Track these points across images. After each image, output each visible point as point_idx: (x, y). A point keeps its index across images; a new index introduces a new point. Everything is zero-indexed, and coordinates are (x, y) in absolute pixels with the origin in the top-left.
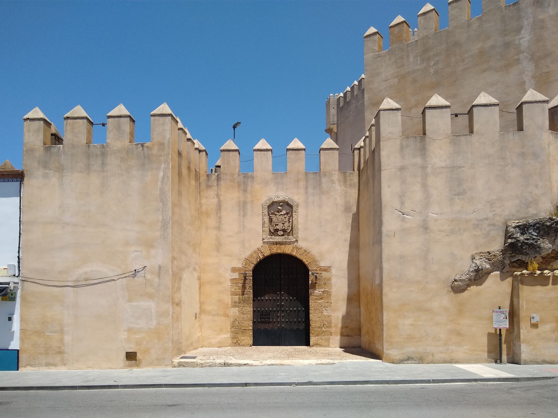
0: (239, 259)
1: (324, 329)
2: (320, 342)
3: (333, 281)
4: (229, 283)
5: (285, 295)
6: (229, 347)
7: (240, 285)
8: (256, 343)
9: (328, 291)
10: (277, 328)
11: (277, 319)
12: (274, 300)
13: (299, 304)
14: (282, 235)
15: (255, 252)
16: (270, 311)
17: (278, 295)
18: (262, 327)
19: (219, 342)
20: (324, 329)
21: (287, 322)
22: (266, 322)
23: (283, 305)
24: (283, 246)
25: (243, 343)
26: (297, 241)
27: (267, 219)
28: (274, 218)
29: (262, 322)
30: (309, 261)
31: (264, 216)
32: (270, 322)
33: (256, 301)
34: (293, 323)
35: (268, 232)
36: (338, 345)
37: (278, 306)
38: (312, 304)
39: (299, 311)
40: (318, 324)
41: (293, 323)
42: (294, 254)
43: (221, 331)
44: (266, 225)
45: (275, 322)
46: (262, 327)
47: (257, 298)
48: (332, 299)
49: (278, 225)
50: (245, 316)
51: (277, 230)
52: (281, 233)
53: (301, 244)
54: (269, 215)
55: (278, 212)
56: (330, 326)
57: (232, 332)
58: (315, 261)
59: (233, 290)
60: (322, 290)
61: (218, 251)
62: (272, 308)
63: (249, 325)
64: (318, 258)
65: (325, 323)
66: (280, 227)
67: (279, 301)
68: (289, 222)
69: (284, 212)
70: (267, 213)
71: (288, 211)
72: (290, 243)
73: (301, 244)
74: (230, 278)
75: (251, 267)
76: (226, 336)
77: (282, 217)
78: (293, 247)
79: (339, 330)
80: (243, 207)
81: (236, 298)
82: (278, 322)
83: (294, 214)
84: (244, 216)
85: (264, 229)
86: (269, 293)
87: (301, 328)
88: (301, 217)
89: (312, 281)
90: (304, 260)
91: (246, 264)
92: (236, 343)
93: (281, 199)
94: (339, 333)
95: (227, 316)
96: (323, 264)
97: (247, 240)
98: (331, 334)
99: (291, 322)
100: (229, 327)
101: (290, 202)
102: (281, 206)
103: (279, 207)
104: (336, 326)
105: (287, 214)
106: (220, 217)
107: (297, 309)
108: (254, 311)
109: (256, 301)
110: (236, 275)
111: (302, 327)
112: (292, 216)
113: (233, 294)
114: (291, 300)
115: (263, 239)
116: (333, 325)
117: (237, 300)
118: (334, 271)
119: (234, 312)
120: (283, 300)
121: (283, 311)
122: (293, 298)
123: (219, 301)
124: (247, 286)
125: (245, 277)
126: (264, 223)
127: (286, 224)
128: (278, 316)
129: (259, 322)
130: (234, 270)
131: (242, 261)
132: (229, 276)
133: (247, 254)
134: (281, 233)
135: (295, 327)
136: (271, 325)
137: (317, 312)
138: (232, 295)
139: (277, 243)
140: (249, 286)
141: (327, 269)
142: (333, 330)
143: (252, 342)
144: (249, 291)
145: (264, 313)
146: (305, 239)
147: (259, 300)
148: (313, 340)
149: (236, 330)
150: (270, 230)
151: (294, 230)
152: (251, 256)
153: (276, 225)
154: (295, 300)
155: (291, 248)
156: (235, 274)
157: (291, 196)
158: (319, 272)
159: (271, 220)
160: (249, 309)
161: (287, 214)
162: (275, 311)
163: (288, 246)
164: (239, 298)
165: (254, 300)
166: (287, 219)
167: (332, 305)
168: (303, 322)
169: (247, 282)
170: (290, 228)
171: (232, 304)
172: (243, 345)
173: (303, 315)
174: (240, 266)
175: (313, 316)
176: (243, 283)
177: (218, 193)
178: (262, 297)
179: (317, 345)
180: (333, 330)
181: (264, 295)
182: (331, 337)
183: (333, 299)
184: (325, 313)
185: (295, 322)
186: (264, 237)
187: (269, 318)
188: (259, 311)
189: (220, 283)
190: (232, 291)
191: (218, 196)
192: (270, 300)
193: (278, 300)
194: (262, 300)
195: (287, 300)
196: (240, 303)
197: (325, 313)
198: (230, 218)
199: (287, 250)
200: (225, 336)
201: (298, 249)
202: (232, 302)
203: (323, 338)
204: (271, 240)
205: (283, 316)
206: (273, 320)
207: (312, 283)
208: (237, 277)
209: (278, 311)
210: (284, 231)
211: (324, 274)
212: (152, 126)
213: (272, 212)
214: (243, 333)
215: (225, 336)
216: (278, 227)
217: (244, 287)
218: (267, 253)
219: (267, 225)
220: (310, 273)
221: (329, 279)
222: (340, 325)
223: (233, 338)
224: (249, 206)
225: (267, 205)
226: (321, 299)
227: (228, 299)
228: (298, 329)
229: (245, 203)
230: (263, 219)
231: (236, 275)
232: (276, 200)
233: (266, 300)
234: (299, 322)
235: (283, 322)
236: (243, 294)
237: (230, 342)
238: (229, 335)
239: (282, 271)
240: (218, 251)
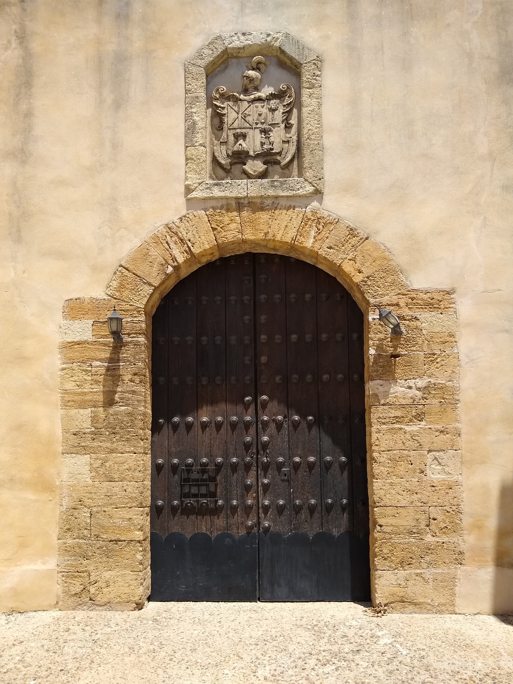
0: (95, 269)
1: (429, 538)
2: (415, 590)
3: (465, 344)
4: (57, 361)
5: (274, 406)
6: (56, 613)
7: (100, 367)
8: (165, 587)
9: (442, 388)
10: (243, 532)
11: (242, 498)
12: (234, 426)
13: (327, 442)
14: (263, 175)
15: (156, 239)
16: (219, 467)
17: (247, 406)
18: (188, 527)
19: (15, 592)
20: (429, 538)
21: (281, 510)
22: (202, 511)
23: (265, 446)
24: (264, 216)
25: (108, 593)
26: (318, 193)
27: (202, 117)
28: (231, 116)
29: (187, 511)
30: (367, 272)
31: (190, 102)
32: (216, 511)
33: (166, 430)
34: (304, 515)
35: (208, 165)
36: (486, 603)
37: (247, 446)
38: (382, 438)
39: (328, 466)
40: (406, 520)
41: (304, 515)
42: (309, 243)
43: (23, 545)
44: (199, 138)
45: (234, 509)
46: (188, 527)
47: (168, 420)
48: (463, 417)
49: (244, 136)
50: (116, 488)
51: (240, 157)
52: (255, 166)
53: (333, 205)
54: (210, 104)
55: (246, 91)
56: (453, 528)
57: (66, 550)
58: (390, 270)
59: (70, 386)
60: (421, 383)
61: (18, 239)
62: (226, 456)
63: (136, 523)
64: (401, 259)
65: (434, 512)
66: (253, 143)
67: (252, 430)
68: (288, 127)
69: (266, 91)
70: (202, 94)
71: (282, 86)
72: (292, 203)
73: (333, 205)
74: (58, 339)
75: (142, 298)
76: (43, 566)
77: (263, 109)
78: (305, 220)
79: (489, 544)
80: (113, 75)
81: (83, 418)
82: (248, 510)
83: (305, 92)
84: (118, 105)
85: (191, 151)
86: (213, 402)
87: (335, 532)
88: (332, 106)
89: (379, 348)
90: (348, 267)
91: (121, 287)
92: (83, 595)
93: (257, 38)
94: (490, 557)
95: (44, 485)
96: (420, 281)
97: (128, 198)
98: (459, 557)
99: (298, 509)
100: (54, 531)
101: (291, 50)
102: (256, 68)
103: (252, 73)
104: (478, 527)
105: (279, 95)
106: (29, 114)
107: (321, 458)
108: (157, 469)
109: (166, 430)
110: (83, 330)
111: (339, 527)
112: (297, 104)
113: (72, 401)
114: (296, 425)
115: (188, 190)
116: (466, 521)
117: (87, 425)
118: (465, 307)
119: (76, 469)
120: (265, 424)
121: (266, 468)
122: (304, 416)
123: (19, 427)
124: (126, 373)
125: (116, 334)
126: (191, 130)
127: (277, 135)
128: (248, 488)
129: (174, 510)
130: (75, 309)
131: (107, 275)
132: (55, 330)
133: (126, 248)
134: (255, 166)
135: (311, 529)
136: (220, 522)
137: (402, 468)
138: (66, 404)
139: (239, 204)
140: (132, 369)
141: (438, 301)
142: (468, 541)
143: (143, 589)
144: (137, 397)
145: (195, 476)
146: (350, 188)
147: (175, 427)
148: (385, 582)
149: (84, 542)
150: (215, 160)
151: (306, 152)
152: (143, 253)
153: (237, 137)
154: (310, 426)
155: (296, 222)
156: (77, 325)
157: (294, 30)
158: (406, 312)
159: (218, 120)
160: (134, 464)
161: (279, 95)
162: (234, 467)
163: (283, 217)
164: (94, 419)
165: (156, 428)
166: (279, 116)
167: (462, 442)
168: (344, 508)
169: (126, 353)
170: (292, 149)
171: (65, 440)
172: (108, 605)
173: (341, 480)
174: (99, 292)
175: (384, 487)
176: (111, 360)
177: (23, 28)
178: (184, 414)
179: (404, 602)
180: (468, 541)
181: (195, 408)
182: (461, 571)
183: (464, 419)
184: (435, 474)
185: (312, 509)
186: (193, 180)
187: (213, 495)
188: (174, 468)
189: (21, 359)
190: (66, 392)
191: (22, 37)
192: (219, 426)
193: (247, 426)
194: (189, 427)
195: (279, 426)
196: (96, 435)
197: (435, 474)
198: (66, 111)
199: (280, 229)
200: (39, 566)
201: (322, 223)
202: (65, 431)
203: (428, 573)
204: (217, 192)
205: (266, 488)
206: (227, 501)
207: (378, 356)
208: (88, 336)
209: (248, 467)
210: (269, 158)
211: (428, 321)
212: (158, 304)
213: (223, 88)
214: (108, 554)
215: (39, 566)
216: (244, 145)
217: (113, 373)
218: (204, 243)
219: (204, 133)
220: (373, 316)
221: (449, 339)
222: (492, 523)
223: (69, 574)
224: (135, 72)
225: (203, 63)
226: (419, 417)
227: (51, 420)
228: (323, 538)
229: (121, 59)
230: (188, 116)
231: (83, 330)
232: (237, 44)
233: (204, 426)
234: (329, 509)
235: (266, 509)
236: (109, 402)
237: (58, 589)
238: (51, 564)
239: (263, 318)
240: (18, 239)
